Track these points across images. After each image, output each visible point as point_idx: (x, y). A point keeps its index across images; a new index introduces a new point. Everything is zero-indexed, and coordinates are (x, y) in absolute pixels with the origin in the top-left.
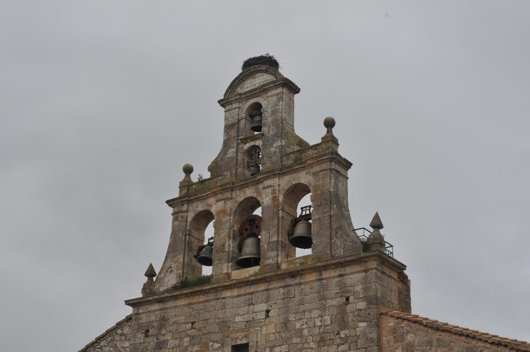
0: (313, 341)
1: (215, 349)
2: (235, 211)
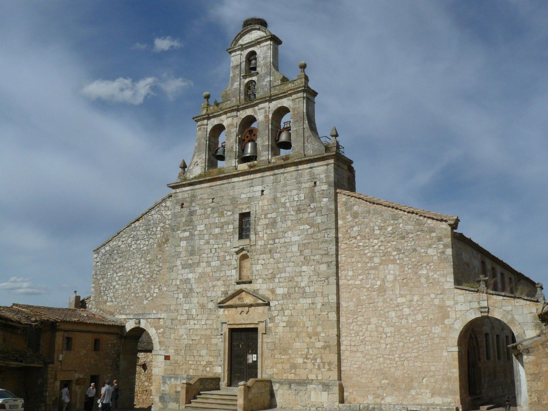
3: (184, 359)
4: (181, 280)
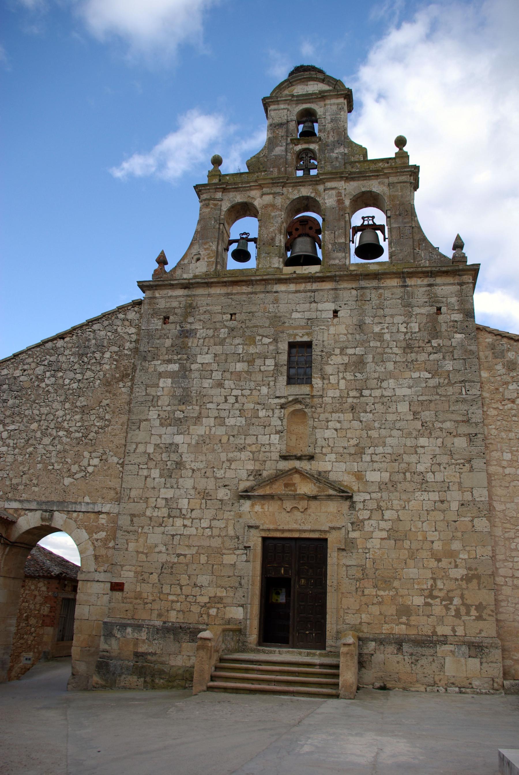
0: (396, 347)
1: (264, 344)
2: (286, 208)
3: (156, 591)
4: (157, 445)
